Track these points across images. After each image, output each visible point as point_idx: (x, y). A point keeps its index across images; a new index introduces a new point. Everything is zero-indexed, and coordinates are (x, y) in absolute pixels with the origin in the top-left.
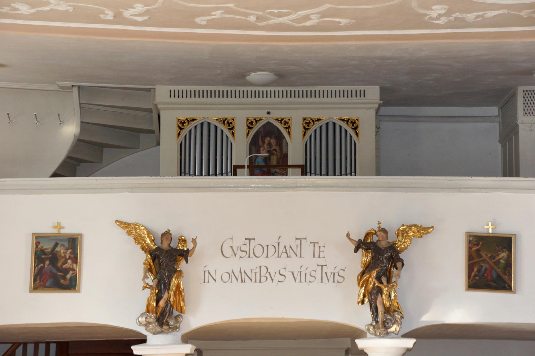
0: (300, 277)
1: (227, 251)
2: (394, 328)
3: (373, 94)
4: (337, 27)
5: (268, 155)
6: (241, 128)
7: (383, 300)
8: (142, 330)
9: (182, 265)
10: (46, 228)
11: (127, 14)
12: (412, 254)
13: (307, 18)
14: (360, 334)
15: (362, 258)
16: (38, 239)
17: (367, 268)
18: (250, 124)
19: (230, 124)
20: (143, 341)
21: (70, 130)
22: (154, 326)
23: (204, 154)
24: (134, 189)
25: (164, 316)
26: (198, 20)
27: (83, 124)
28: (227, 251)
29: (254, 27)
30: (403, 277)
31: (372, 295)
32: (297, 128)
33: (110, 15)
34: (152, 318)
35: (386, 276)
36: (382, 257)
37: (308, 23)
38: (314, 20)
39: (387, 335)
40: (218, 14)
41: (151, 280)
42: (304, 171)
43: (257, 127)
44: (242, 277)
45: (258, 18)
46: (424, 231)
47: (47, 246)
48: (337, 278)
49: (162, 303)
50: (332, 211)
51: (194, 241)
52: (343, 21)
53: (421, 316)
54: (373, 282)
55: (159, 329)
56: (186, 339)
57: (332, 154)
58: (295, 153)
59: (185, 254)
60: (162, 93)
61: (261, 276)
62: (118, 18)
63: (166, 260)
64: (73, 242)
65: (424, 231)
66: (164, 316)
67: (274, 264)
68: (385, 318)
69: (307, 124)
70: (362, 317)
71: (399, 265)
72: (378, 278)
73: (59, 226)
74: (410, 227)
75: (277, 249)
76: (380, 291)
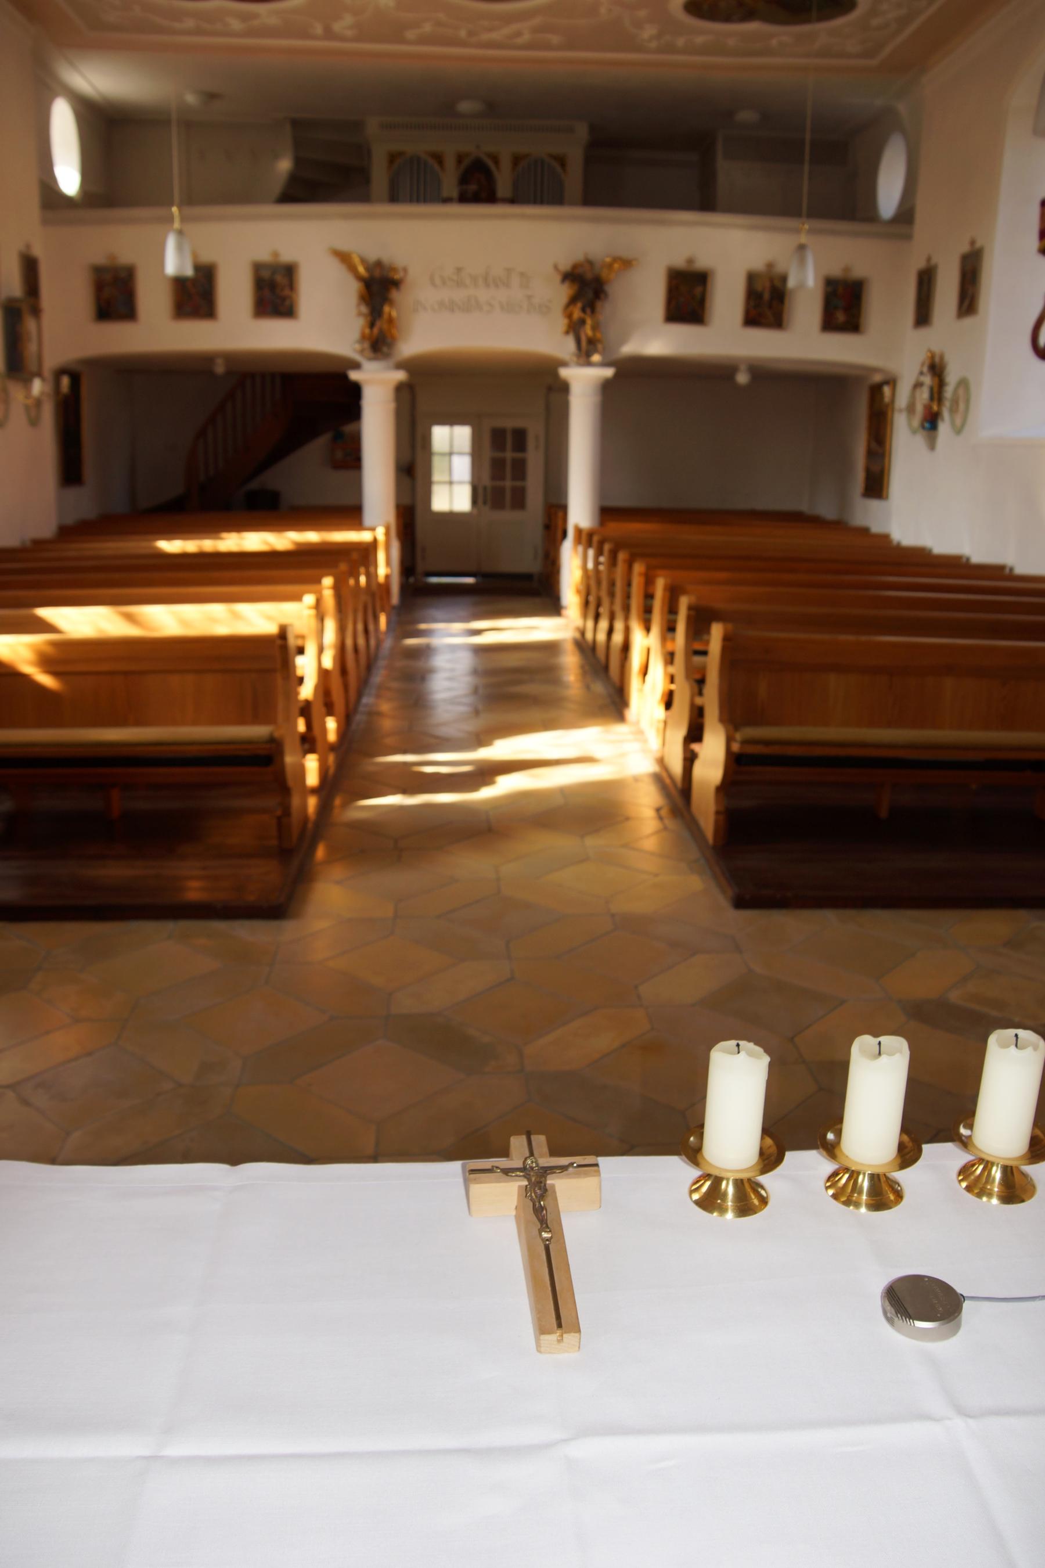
0: (509, 308)
1: (438, 281)
2: (596, 358)
3: (582, 131)
4: (548, 47)
5: (478, 186)
6: (450, 163)
7: (588, 330)
8: (357, 357)
9: (394, 294)
10: (264, 256)
11: (337, 27)
12: (616, 289)
13: (519, 34)
14: (564, 364)
15: (563, 293)
16: (258, 268)
17: (573, 301)
18: (460, 158)
19: (439, 158)
20: (357, 366)
21: (285, 165)
22: (368, 353)
23: (412, 184)
24: (346, 217)
25: (379, 343)
26: (410, 34)
27: (298, 161)
28: (438, 281)
29: (463, 44)
30: (605, 310)
31: (574, 328)
32: (506, 163)
33: (319, 30)
34: (367, 345)
35: (590, 307)
36: (588, 289)
37: (519, 41)
38: (526, 37)
39: (589, 364)
40: (427, 28)
41: (364, 309)
42: (512, 201)
43: (467, 162)
44: (451, 307)
45: (471, 34)
46: (627, 264)
47: (266, 274)
48: (544, 310)
49: (376, 330)
50: (539, 241)
51: (405, 270)
52: (555, 39)
53: (623, 341)
54: (577, 314)
55: (372, 355)
56: (399, 366)
57: (537, 186)
58: (503, 183)
59: (396, 284)
60: (372, 127)
61: (469, 306)
62: (329, 34)
63: (379, 288)
64: (290, 271)
65: (627, 264)
66: (379, 343)
67: (483, 294)
68: (586, 351)
69: (516, 160)
70: (563, 347)
71: (602, 296)
72: (583, 310)
73: (276, 254)
74: (615, 259)
75: (486, 279)
76: (583, 322)
